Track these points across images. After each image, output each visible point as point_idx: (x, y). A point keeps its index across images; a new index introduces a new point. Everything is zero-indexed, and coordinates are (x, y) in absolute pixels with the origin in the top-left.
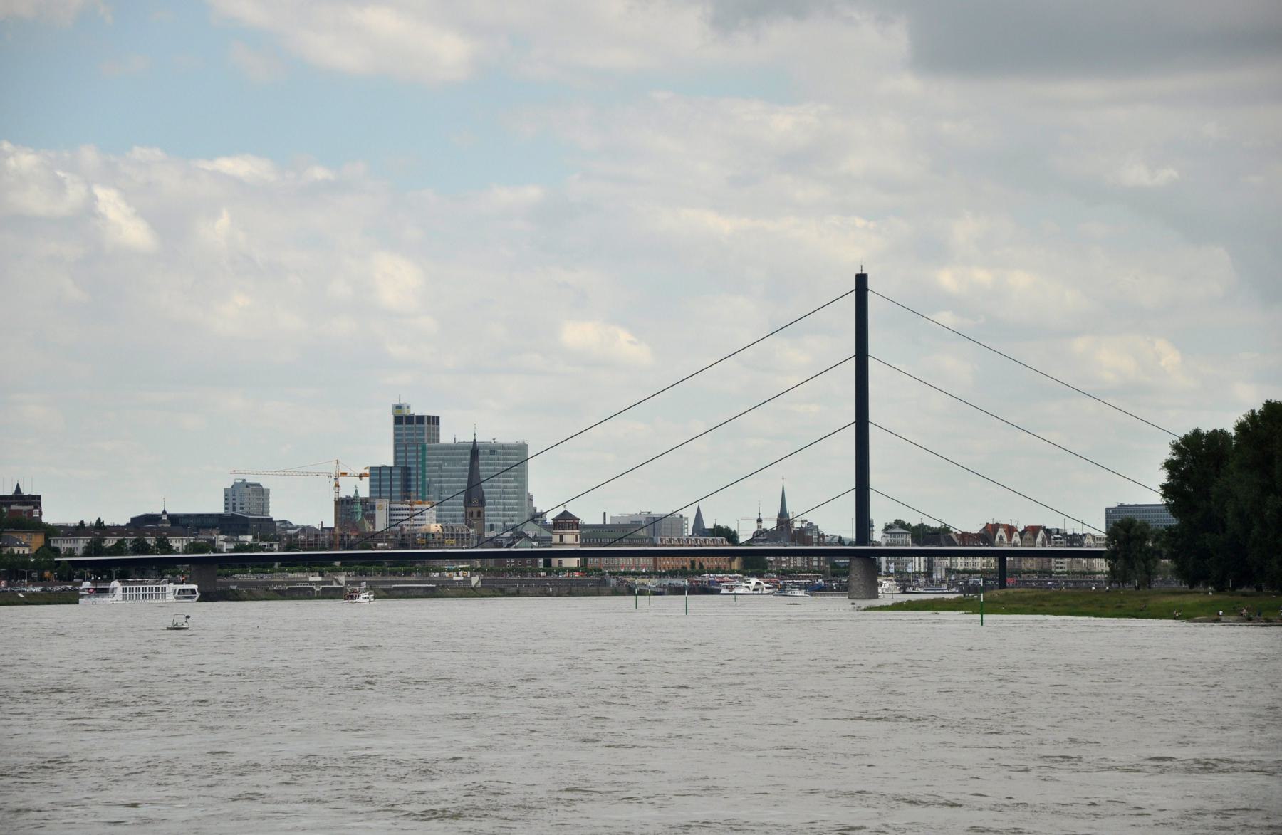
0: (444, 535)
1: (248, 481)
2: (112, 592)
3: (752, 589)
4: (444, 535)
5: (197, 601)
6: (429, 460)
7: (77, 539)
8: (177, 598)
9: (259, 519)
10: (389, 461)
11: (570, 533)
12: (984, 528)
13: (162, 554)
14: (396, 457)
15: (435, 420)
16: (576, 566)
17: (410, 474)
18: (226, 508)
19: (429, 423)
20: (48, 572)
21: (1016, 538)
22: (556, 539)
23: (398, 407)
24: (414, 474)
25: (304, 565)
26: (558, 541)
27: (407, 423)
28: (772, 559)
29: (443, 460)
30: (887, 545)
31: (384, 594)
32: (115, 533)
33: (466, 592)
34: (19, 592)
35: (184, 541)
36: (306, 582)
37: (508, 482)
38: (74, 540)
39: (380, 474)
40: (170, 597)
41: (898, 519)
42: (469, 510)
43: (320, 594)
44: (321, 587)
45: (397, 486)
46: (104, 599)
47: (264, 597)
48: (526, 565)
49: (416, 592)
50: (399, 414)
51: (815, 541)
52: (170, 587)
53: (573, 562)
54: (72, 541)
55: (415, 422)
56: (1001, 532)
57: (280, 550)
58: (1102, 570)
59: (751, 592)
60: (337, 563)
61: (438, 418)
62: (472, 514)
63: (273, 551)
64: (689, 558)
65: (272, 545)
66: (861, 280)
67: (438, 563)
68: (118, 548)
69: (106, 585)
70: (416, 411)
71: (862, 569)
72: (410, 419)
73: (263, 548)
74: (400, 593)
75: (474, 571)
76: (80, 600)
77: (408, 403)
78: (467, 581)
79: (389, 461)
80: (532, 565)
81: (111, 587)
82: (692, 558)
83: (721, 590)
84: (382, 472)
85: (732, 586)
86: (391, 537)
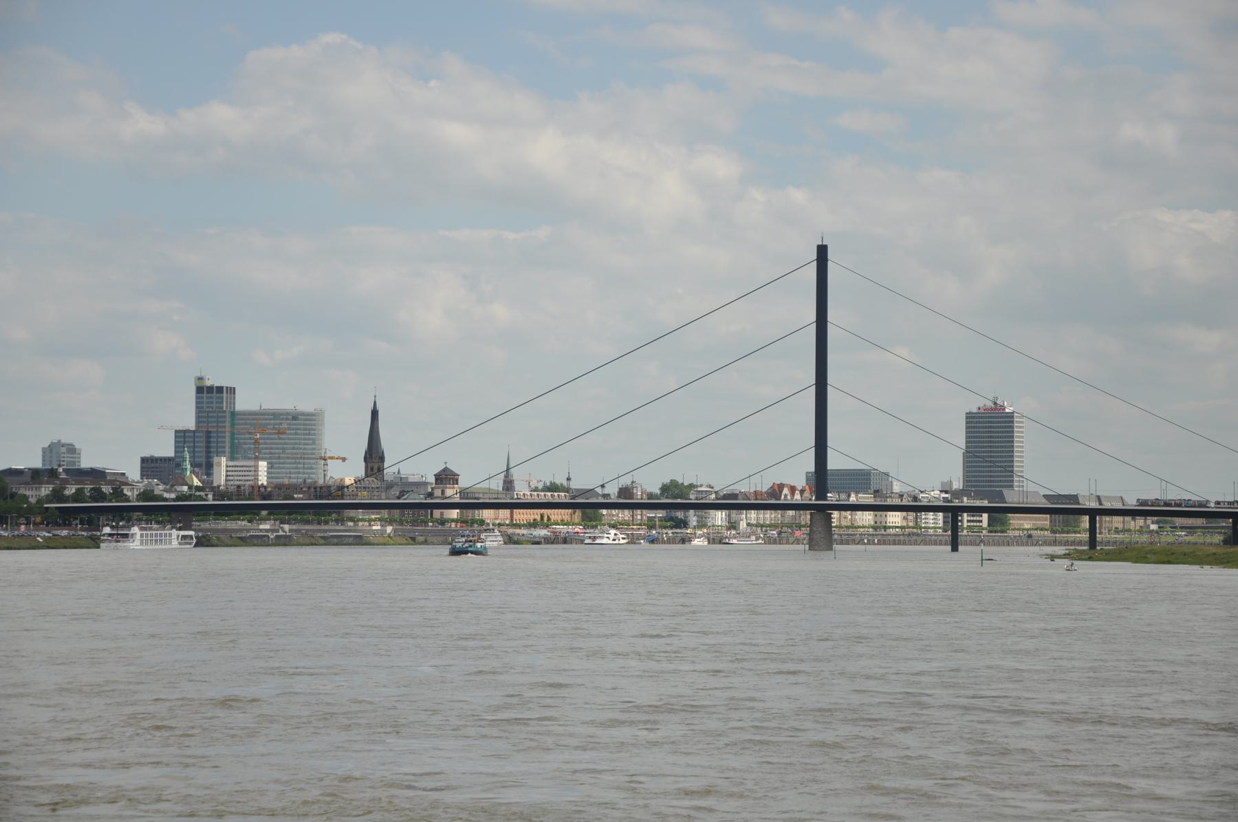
0: (357, 488)
1: (62, 441)
2: (132, 537)
3: (611, 539)
4: (357, 488)
5: (195, 546)
6: (239, 424)
7: (39, 488)
8: (180, 544)
9: (114, 473)
12: (771, 487)
13: (116, 502)
15: (232, 391)
16: (456, 517)
17: (210, 437)
18: (43, 464)
20: (40, 518)
21: (797, 496)
22: (438, 493)
23: (200, 379)
24: (214, 437)
25: (239, 514)
26: (440, 495)
27: (217, 392)
28: (604, 512)
29: (250, 424)
30: (697, 499)
31: (322, 541)
32: (73, 482)
33: (383, 542)
34: (38, 536)
35: (135, 490)
36: (257, 530)
37: (307, 444)
38: (36, 488)
39: (184, 437)
40: (175, 543)
41: (673, 479)
42: (370, 465)
43: (274, 541)
44: (275, 534)
46: (125, 544)
47: (230, 543)
48: (419, 515)
49: (347, 540)
50: (200, 385)
51: (639, 497)
52: (175, 533)
53: (454, 514)
54: (34, 489)
55: (205, 392)
56: (786, 491)
57: (214, 500)
58: (1134, 519)
59: (611, 542)
60: (264, 513)
61: (234, 388)
62: (372, 469)
63: (207, 501)
64: (539, 511)
65: (206, 495)
66: (822, 251)
67: (352, 513)
68: (78, 496)
69: (127, 530)
71: (823, 523)
72: (210, 389)
73: (200, 498)
74: (335, 540)
75: (391, 522)
76: (102, 544)
78: (383, 532)
80: (424, 516)
81: (132, 532)
82: (543, 511)
83: (1226, 542)
85: (594, 537)
86: (304, 489)
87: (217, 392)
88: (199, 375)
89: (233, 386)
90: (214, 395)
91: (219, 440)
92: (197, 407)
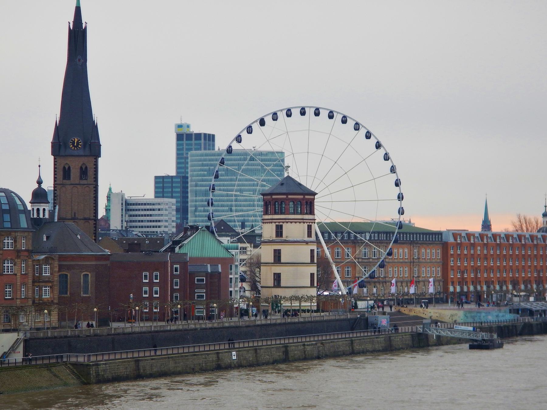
10: (172, 172)
11: (295, 221)
14: (178, 168)
19: (205, 139)
23: (180, 126)
27: (196, 139)
39: (163, 182)
45: (177, 187)
70: (195, 129)
72: (189, 136)
77: (188, 123)
79: (172, 172)
84: (165, 180)
87: (196, 139)
88: (179, 122)
89: (211, 133)
90: (193, 142)
91: (161, 185)
92: (178, 154)
